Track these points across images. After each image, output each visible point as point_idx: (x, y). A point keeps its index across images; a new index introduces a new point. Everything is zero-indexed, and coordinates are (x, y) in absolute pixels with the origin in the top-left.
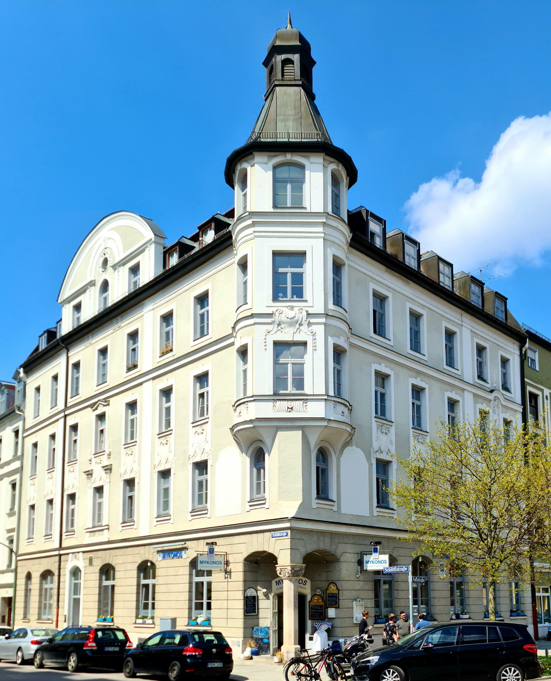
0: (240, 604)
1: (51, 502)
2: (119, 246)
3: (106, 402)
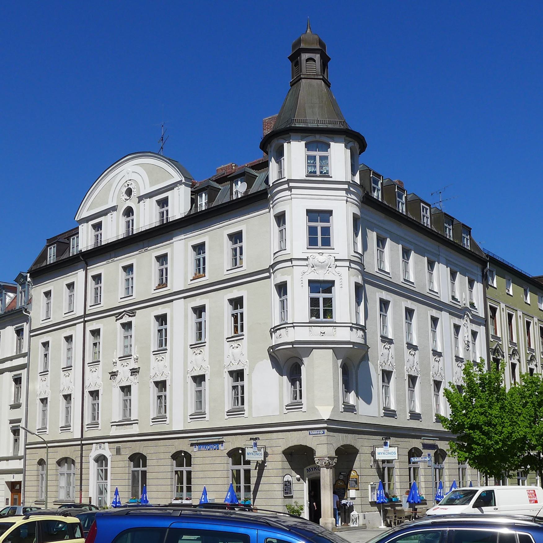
0: (280, 487)
1: (68, 397)
2: (136, 186)
3: (133, 313)
